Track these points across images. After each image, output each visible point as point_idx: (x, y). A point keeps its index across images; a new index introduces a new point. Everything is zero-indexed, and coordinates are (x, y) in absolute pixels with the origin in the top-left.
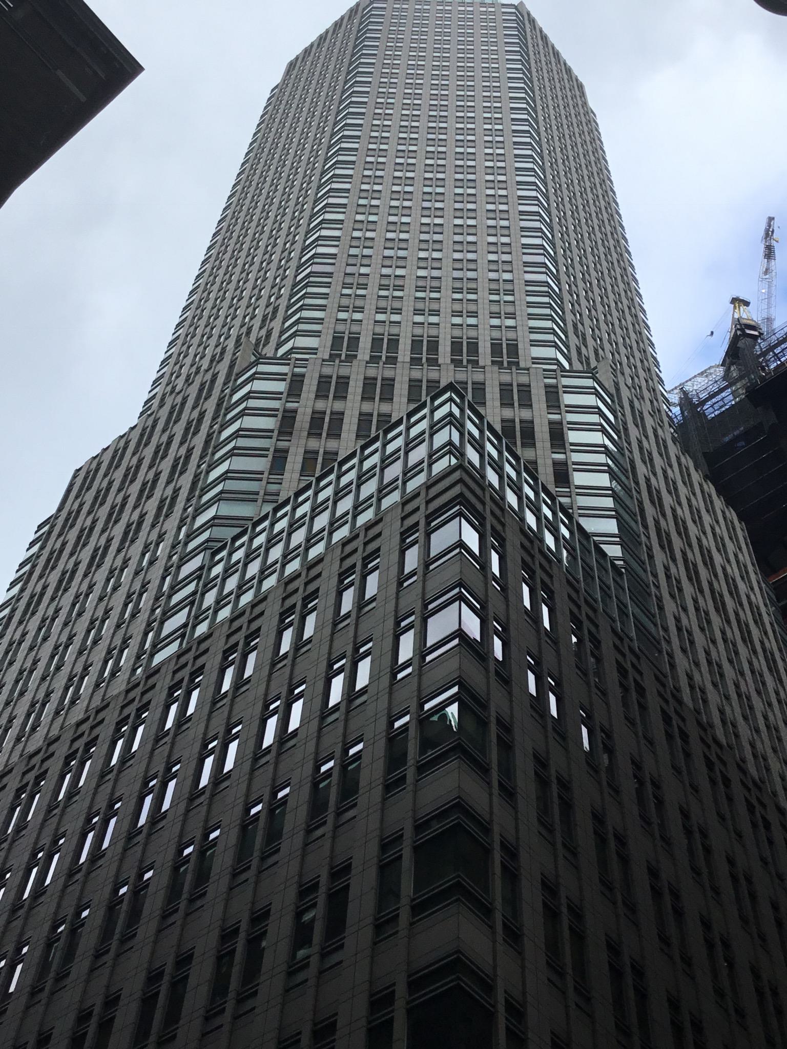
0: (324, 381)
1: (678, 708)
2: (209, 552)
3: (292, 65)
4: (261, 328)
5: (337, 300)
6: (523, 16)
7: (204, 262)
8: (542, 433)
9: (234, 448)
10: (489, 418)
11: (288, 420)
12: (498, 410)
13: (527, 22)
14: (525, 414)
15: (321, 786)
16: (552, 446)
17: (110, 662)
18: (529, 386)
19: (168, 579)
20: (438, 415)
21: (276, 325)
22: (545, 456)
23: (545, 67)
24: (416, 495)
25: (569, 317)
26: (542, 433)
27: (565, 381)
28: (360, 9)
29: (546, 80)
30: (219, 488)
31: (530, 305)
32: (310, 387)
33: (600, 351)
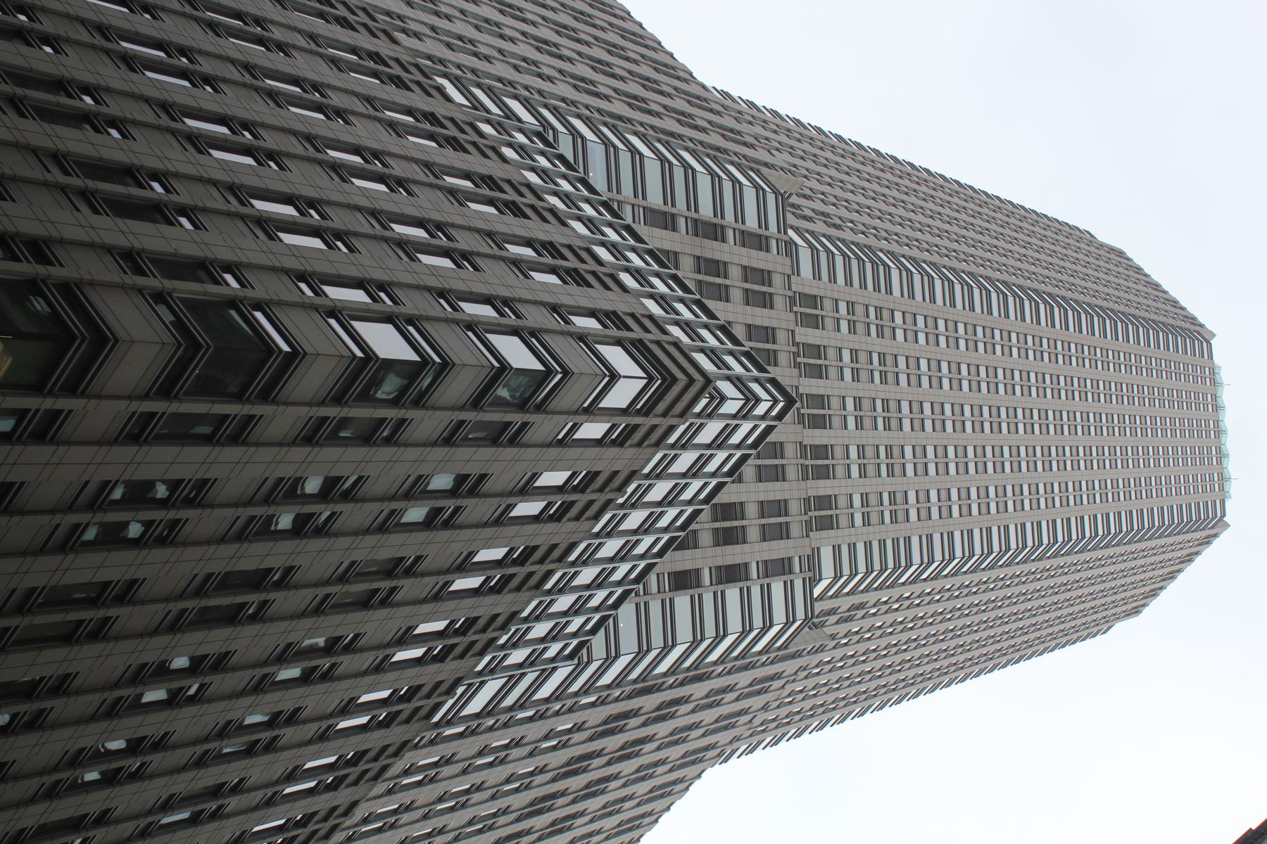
0: (764, 276)
1: (370, 775)
2: (541, 129)
3: (1120, 253)
4: (813, 210)
5: (860, 300)
6: (1212, 527)
7: (877, 152)
8: (732, 555)
9: (670, 163)
10: (780, 427)
11: (714, 231)
12: (754, 497)
13: (1204, 534)
14: (753, 533)
15: (233, 313)
16: (719, 568)
17: (358, 159)
18: (788, 538)
19: (467, 184)
20: (755, 387)
21: (819, 227)
22: (706, 558)
23: (1119, 597)
24: (665, 332)
25: (871, 597)
26: (732, 555)
27: (798, 584)
28: (1198, 328)
29: (1103, 601)
30: (620, 146)
31: (882, 544)
32: (756, 259)
33: (861, 613)
